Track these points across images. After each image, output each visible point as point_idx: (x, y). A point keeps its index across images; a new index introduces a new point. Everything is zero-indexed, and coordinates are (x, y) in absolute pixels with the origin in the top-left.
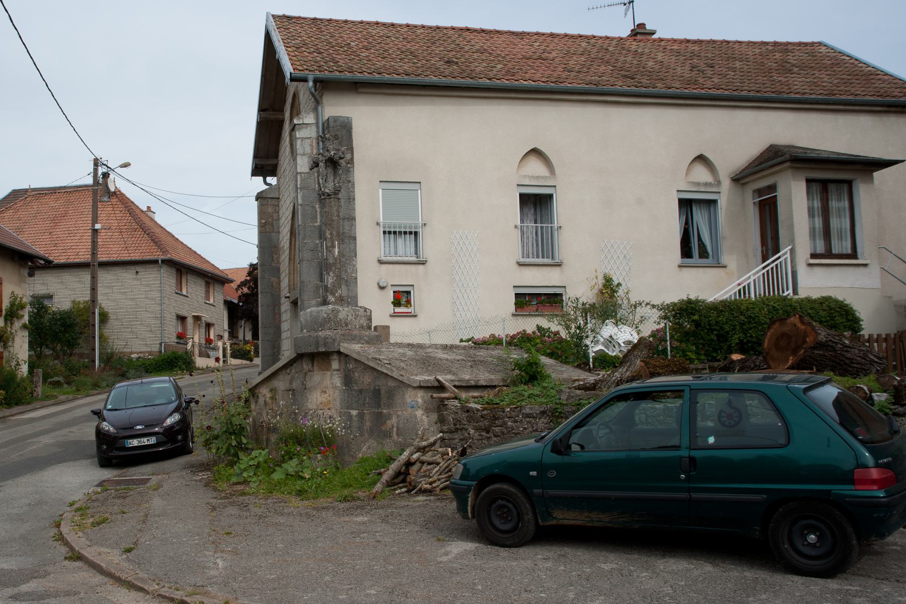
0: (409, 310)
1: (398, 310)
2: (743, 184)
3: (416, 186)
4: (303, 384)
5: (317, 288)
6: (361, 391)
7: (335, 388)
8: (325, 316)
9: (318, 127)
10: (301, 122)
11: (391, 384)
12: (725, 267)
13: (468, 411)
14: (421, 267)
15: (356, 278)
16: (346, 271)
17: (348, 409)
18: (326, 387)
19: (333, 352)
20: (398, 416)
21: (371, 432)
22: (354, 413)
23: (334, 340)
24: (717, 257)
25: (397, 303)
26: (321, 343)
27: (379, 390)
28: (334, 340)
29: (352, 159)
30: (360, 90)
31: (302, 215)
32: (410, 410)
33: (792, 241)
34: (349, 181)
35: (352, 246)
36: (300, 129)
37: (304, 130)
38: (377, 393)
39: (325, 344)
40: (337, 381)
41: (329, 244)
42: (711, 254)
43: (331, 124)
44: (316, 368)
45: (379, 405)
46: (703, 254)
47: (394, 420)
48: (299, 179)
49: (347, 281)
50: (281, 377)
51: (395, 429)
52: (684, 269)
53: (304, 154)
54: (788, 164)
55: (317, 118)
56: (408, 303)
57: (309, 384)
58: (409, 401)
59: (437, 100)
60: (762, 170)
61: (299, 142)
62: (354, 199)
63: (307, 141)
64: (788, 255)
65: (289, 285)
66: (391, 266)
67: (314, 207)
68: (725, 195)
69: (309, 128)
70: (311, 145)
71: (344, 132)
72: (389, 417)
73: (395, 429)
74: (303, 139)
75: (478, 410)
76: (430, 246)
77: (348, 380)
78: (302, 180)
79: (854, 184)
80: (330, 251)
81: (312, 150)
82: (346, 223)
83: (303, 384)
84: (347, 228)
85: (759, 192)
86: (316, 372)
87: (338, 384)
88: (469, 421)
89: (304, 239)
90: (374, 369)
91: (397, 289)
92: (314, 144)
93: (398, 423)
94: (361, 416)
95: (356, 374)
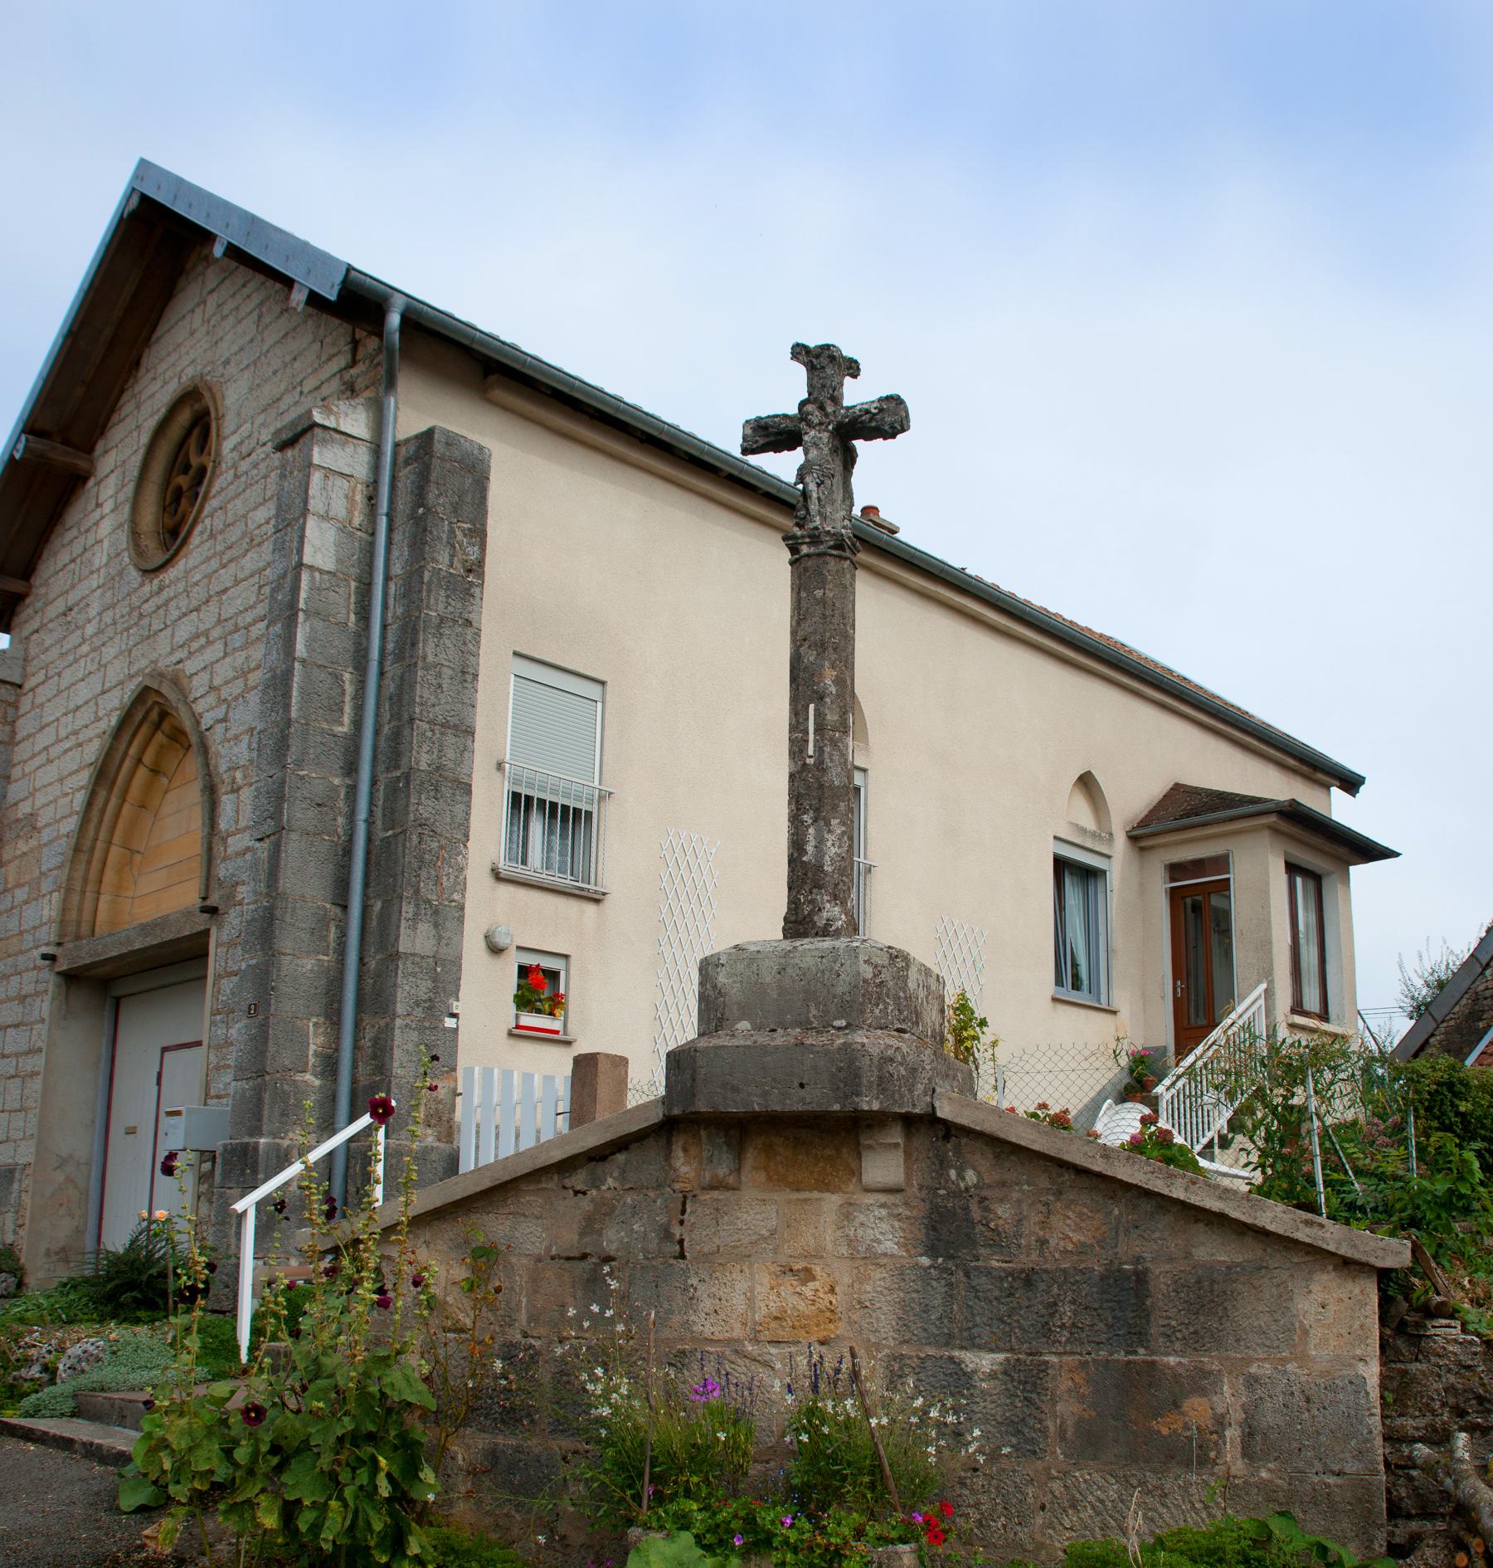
0: (556, 1025)
1: (529, 1019)
2: (1142, 849)
3: (593, 691)
4: (667, 1235)
6: (1028, 1279)
7: (872, 1258)
11: (1212, 1251)
12: (1114, 1013)
14: (590, 908)
16: (438, 881)
17: (949, 1341)
18: (818, 1255)
20: (1252, 1381)
21: (1088, 1443)
22: (983, 1362)
23: (913, 1071)
24: (1094, 989)
25: (524, 1002)
26: (870, 1076)
28: (913, 1071)
29: (481, 562)
30: (499, 394)
31: (302, 691)
33: (1267, 974)
34: (469, 623)
35: (459, 809)
36: (324, 442)
37: (337, 449)
38: (1126, 1292)
39: (883, 1083)
40: (885, 1232)
41: (832, 717)
42: (1086, 982)
43: (438, 447)
44: (747, 1175)
45: (1138, 1336)
46: (1076, 985)
47: (1229, 1397)
49: (436, 912)
50: (531, 1200)
51: (1232, 1433)
52: (1061, 1008)
53: (326, 517)
54: (1273, 819)
55: (379, 425)
56: (556, 1003)
57: (700, 1234)
59: (660, 486)
61: (316, 478)
64: (1262, 1002)
65: (63, 923)
67: (337, 678)
69: (350, 449)
71: (469, 481)
72: (1201, 1382)
73: (1232, 1433)
74: (329, 472)
76: (618, 854)
77: (946, 1231)
79: (1325, 883)
80: (834, 743)
81: (350, 512)
82: (450, 739)
83: (667, 1235)
84: (451, 754)
85: (1176, 870)
86: (749, 1193)
87: (889, 1246)
90: (1148, 1194)
91: (531, 960)
92: (359, 498)
94: (1025, 1380)
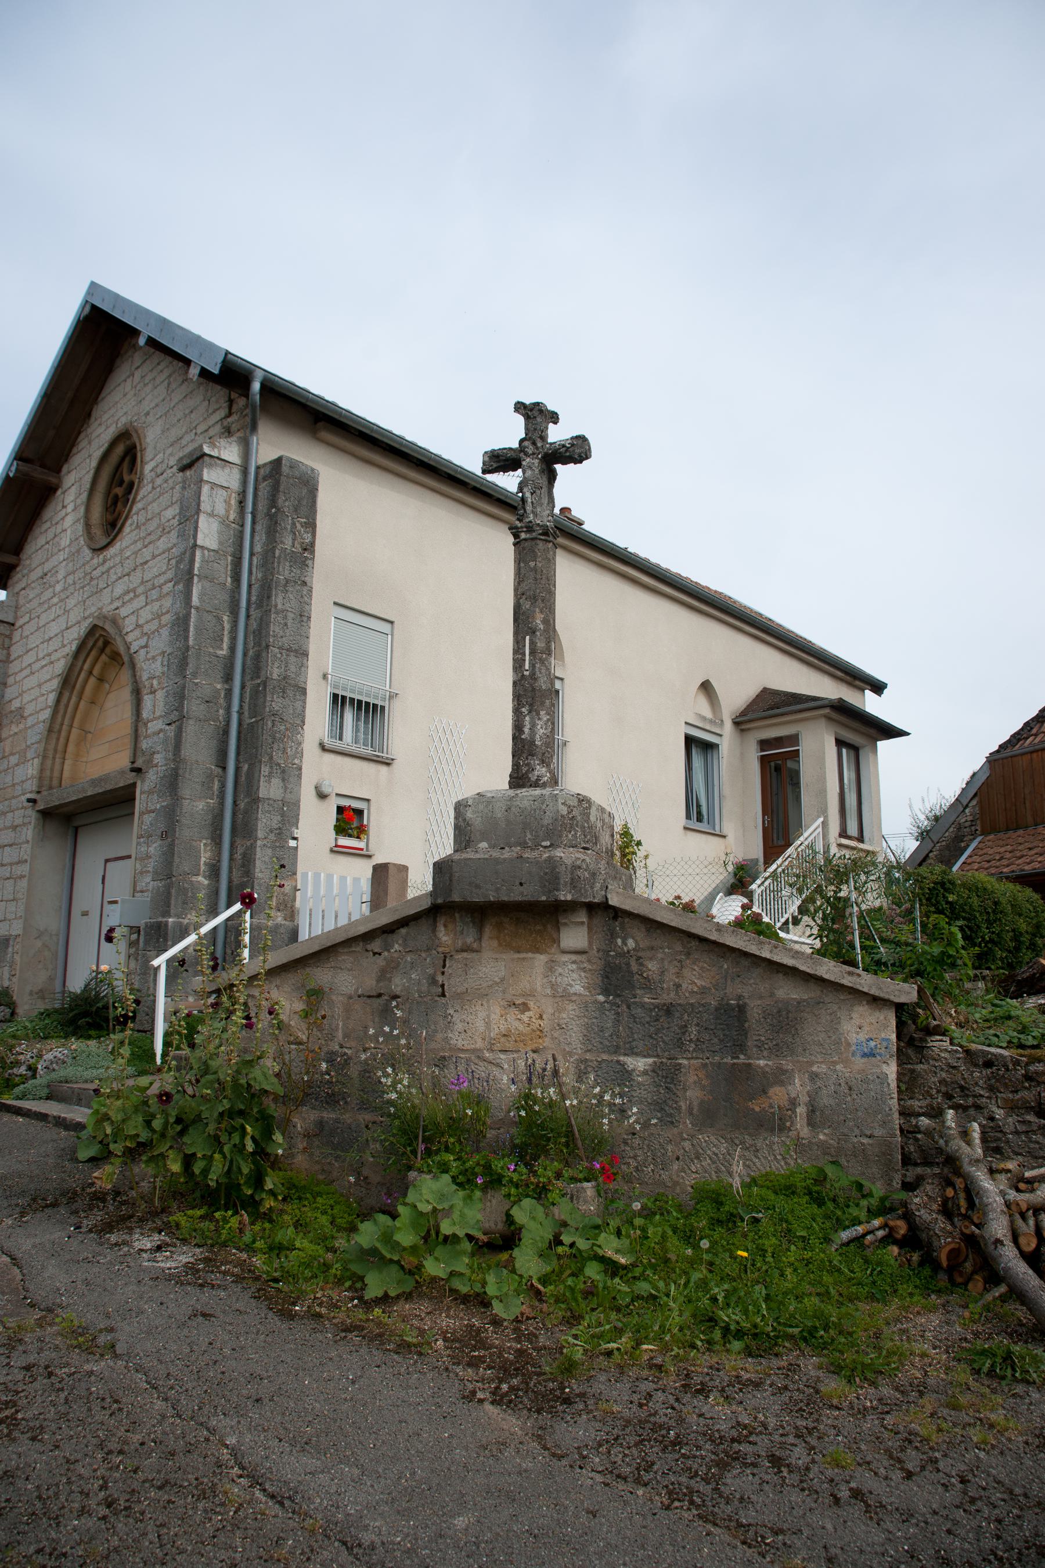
0: (361, 844)
1: (344, 841)
2: (742, 730)
3: (385, 627)
4: (433, 981)
5: (210, 777)
8: (564, 810)
9: (245, 472)
10: (215, 453)
11: (788, 992)
13: (988, 1064)
14: (384, 769)
15: (300, 769)
16: (284, 751)
17: (617, 1050)
18: (532, 994)
19: (571, 907)
20: (814, 1077)
22: (639, 1064)
24: (711, 822)
25: (341, 829)
27: (742, 1009)
29: (312, 544)
31: (197, 628)
32: (859, 1062)
33: (824, 811)
34: (304, 583)
36: (210, 466)
37: (219, 470)
39: (574, 883)
40: (575, 979)
42: (706, 817)
43: (285, 469)
45: (740, 1047)
47: (799, 1087)
48: (198, 558)
49: (283, 772)
52: (690, 834)
53: (212, 515)
54: (827, 711)
55: (246, 455)
56: (361, 831)
57: (455, 980)
58: (853, 1038)
60: (771, 717)
62: (309, 618)
63: (221, 492)
64: (820, 830)
66: (339, 759)
67: (219, 619)
68: (727, 739)
69: (227, 470)
70: (227, 502)
71: (305, 491)
72: (780, 1077)
74: (214, 485)
75: (1017, 1063)
76: (402, 734)
77: (615, 979)
78: (203, 561)
79: (861, 753)
81: (227, 511)
82: (292, 659)
84: (293, 668)
85: (764, 744)
86: (487, 954)
87: (578, 988)
88: (991, 1089)
89: (195, 675)
90: (746, 954)
92: (233, 502)
93: (813, 1097)
94: (667, 1076)
95: (652, 966)
